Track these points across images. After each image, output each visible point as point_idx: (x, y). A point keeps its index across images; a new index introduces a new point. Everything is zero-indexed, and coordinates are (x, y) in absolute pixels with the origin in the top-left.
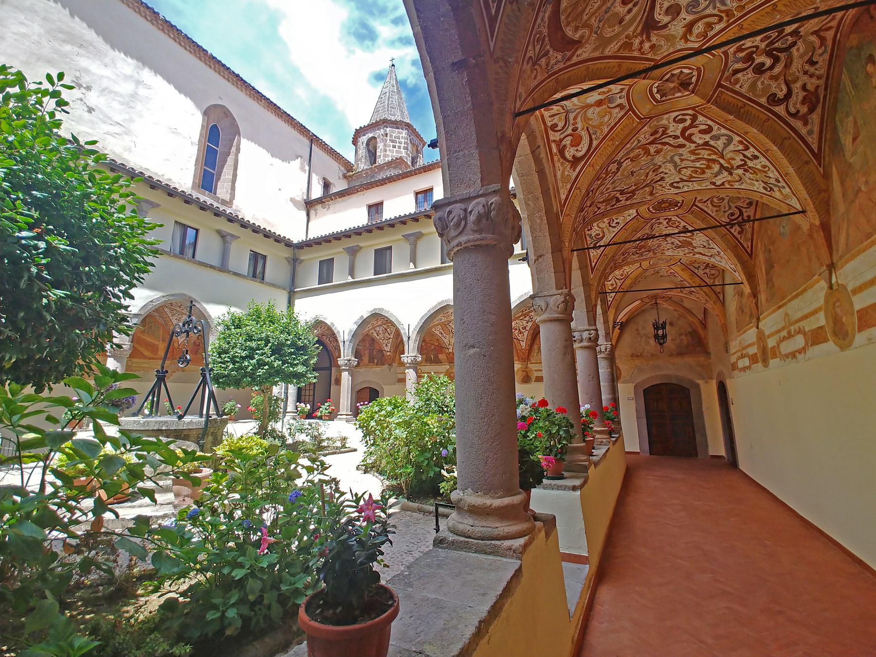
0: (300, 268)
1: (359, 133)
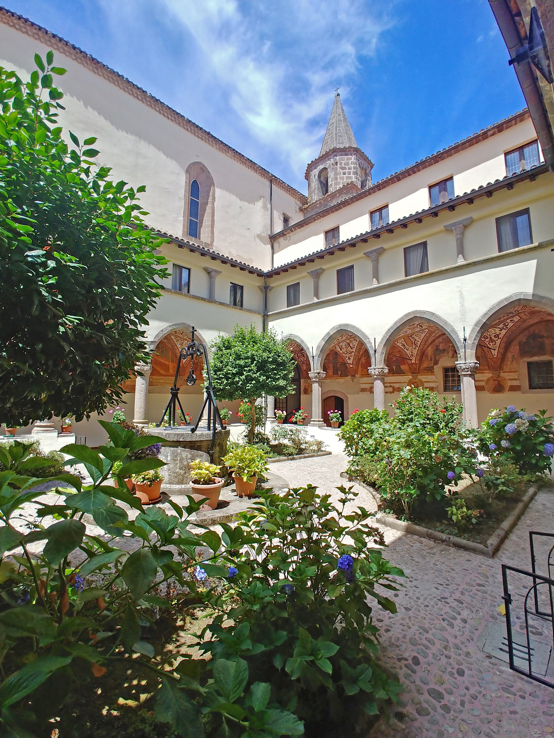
0: (270, 295)
1: (311, 167)
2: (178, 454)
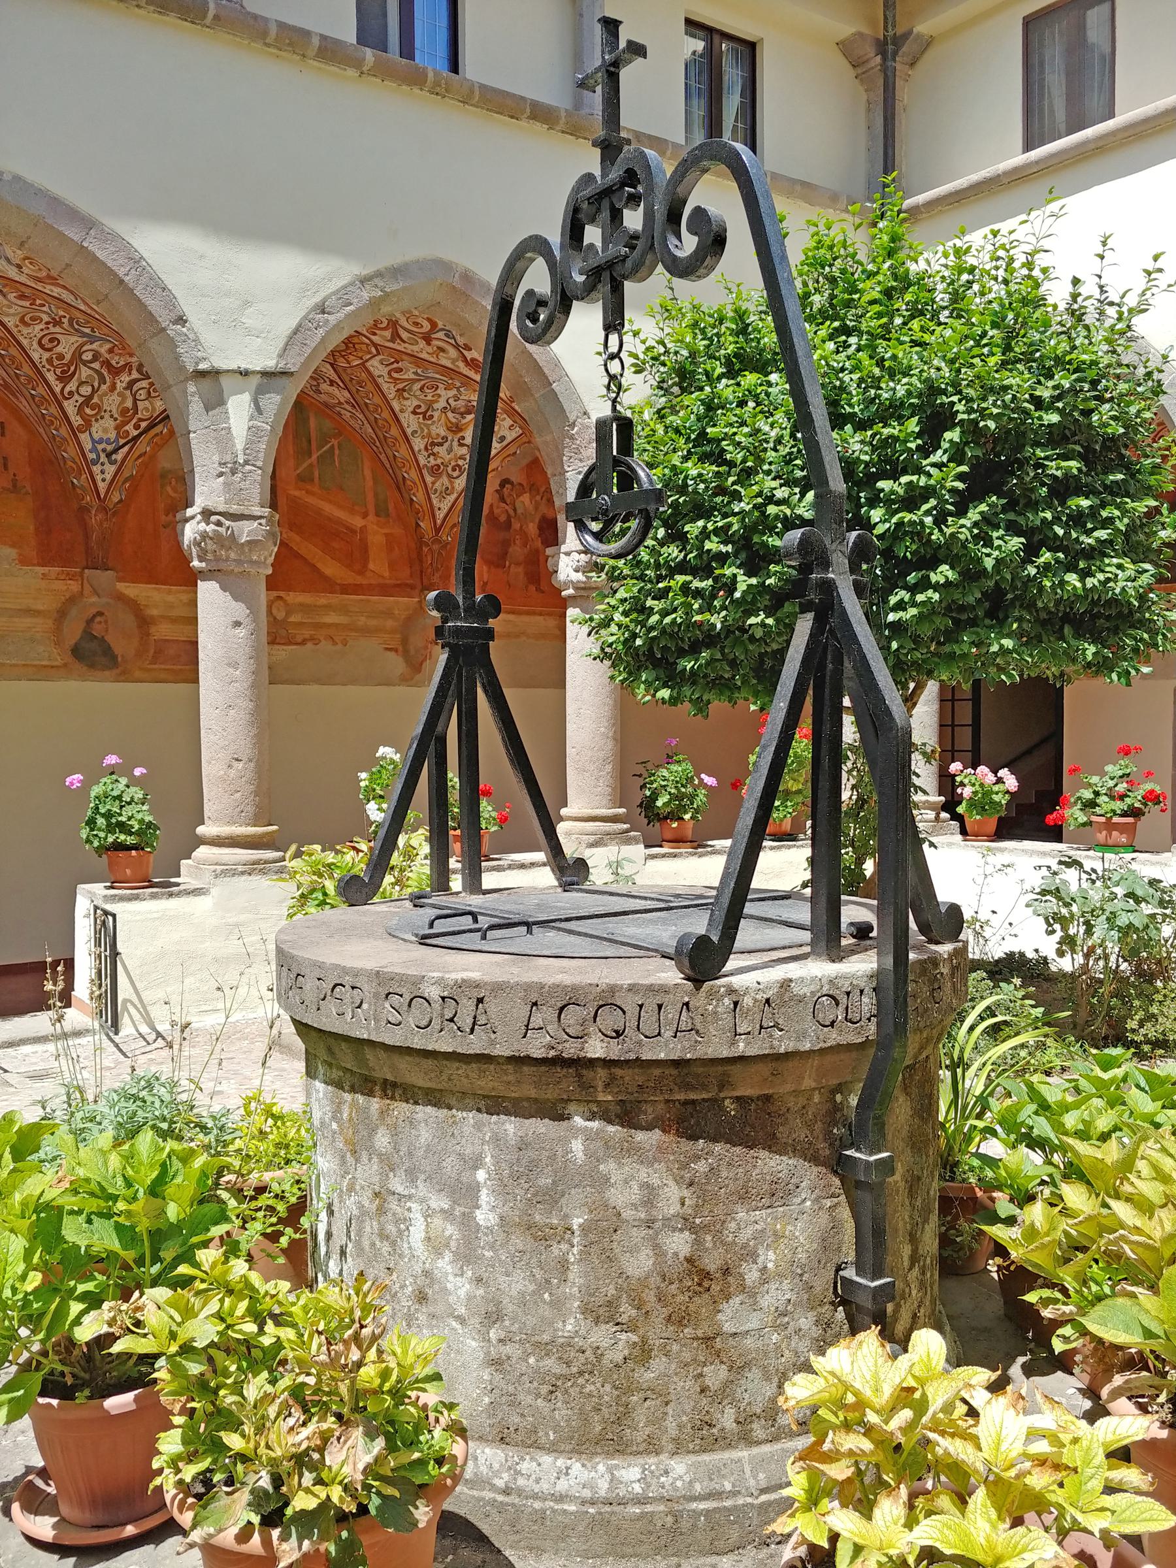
2: (566, 1178)
